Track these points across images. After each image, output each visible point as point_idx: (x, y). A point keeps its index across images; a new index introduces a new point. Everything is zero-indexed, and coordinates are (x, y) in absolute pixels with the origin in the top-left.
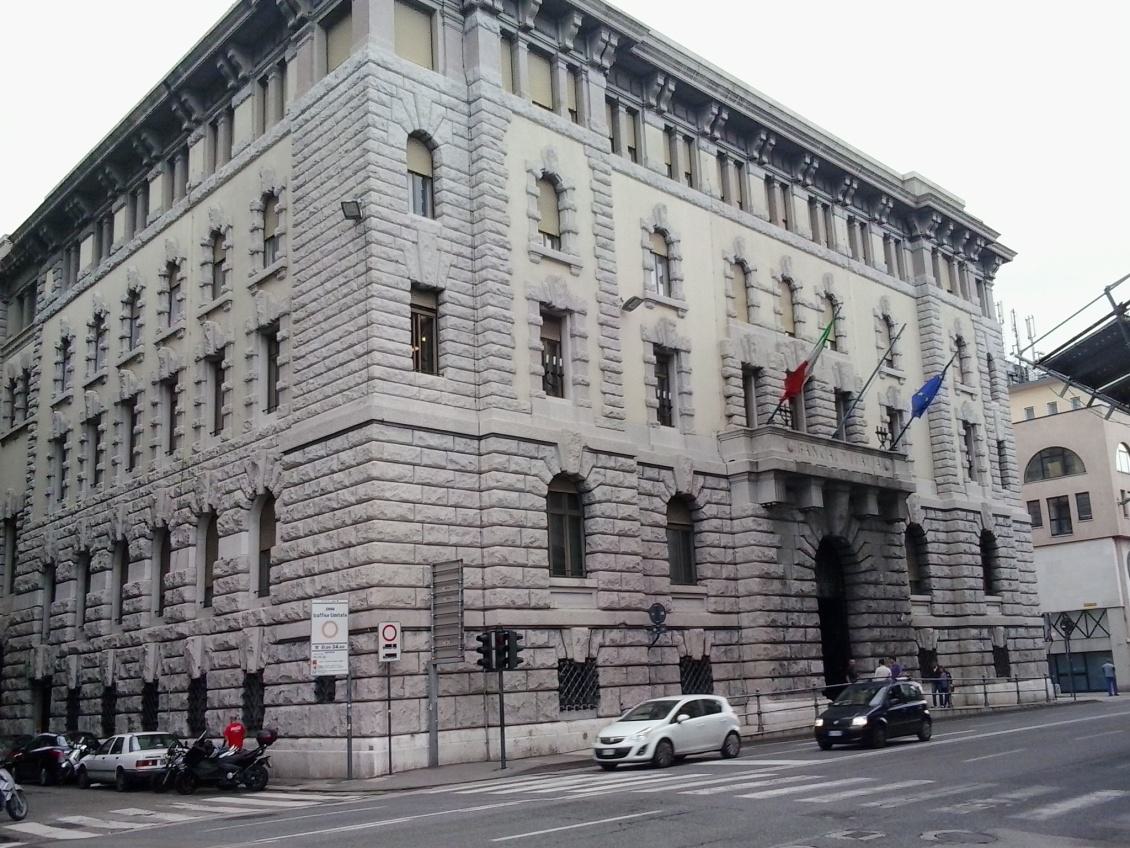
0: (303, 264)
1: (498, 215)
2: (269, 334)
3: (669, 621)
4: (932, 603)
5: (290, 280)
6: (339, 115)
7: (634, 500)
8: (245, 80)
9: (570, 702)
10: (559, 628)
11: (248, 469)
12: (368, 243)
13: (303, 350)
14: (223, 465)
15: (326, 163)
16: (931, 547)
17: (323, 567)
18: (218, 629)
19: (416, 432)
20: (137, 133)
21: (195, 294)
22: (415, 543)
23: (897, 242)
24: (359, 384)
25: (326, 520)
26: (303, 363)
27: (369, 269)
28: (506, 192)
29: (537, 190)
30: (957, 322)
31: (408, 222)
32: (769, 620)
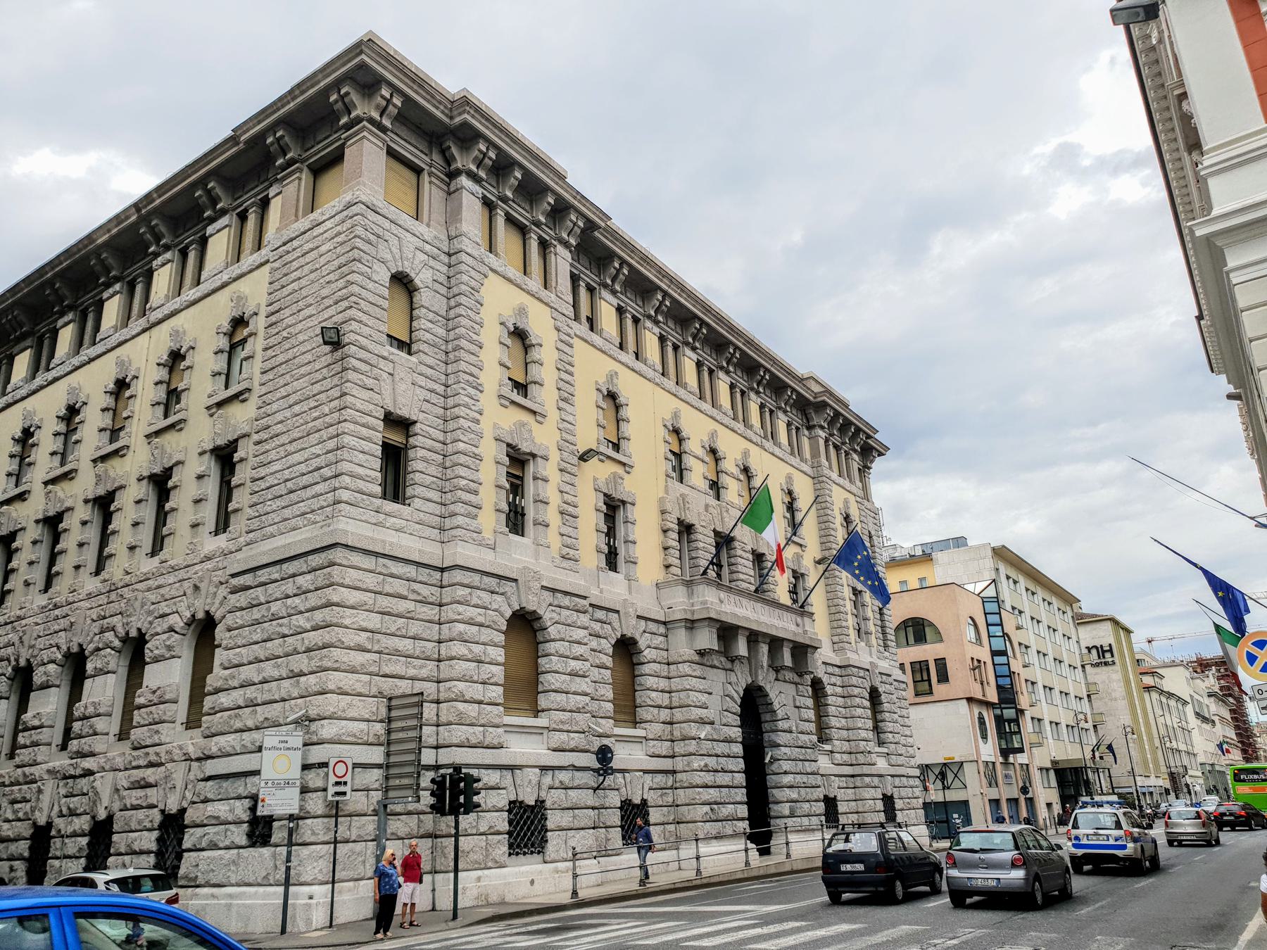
0: (270, 386)
1: (472, 359)
2: (225, 457)
3: (615, 764)
4: (832, 752)
5: (254, 401)
6: (323, 249)
7: (585, 640)
8: (224, 212)
9: (518, 846)
10: (512, 768)
11: (189, 592)
12: (345, 369)
13: (262, 472)
14: (159, 587)
15: (304, 293)
16: (831, 700)
17: (267, 697)
18: (134, 764)
19: (381, 560)
20: (97, 252)
21: (91, 438)
22: (370, 674)
23: (797, 429)
24: (322, 508)
25: (274, 647)
26: (263, 485)
27: (343, 394)
28: (482, 339)
29: (509, 342)
30: (846, 502)
31: (386, 354)
32: (702, 764)
